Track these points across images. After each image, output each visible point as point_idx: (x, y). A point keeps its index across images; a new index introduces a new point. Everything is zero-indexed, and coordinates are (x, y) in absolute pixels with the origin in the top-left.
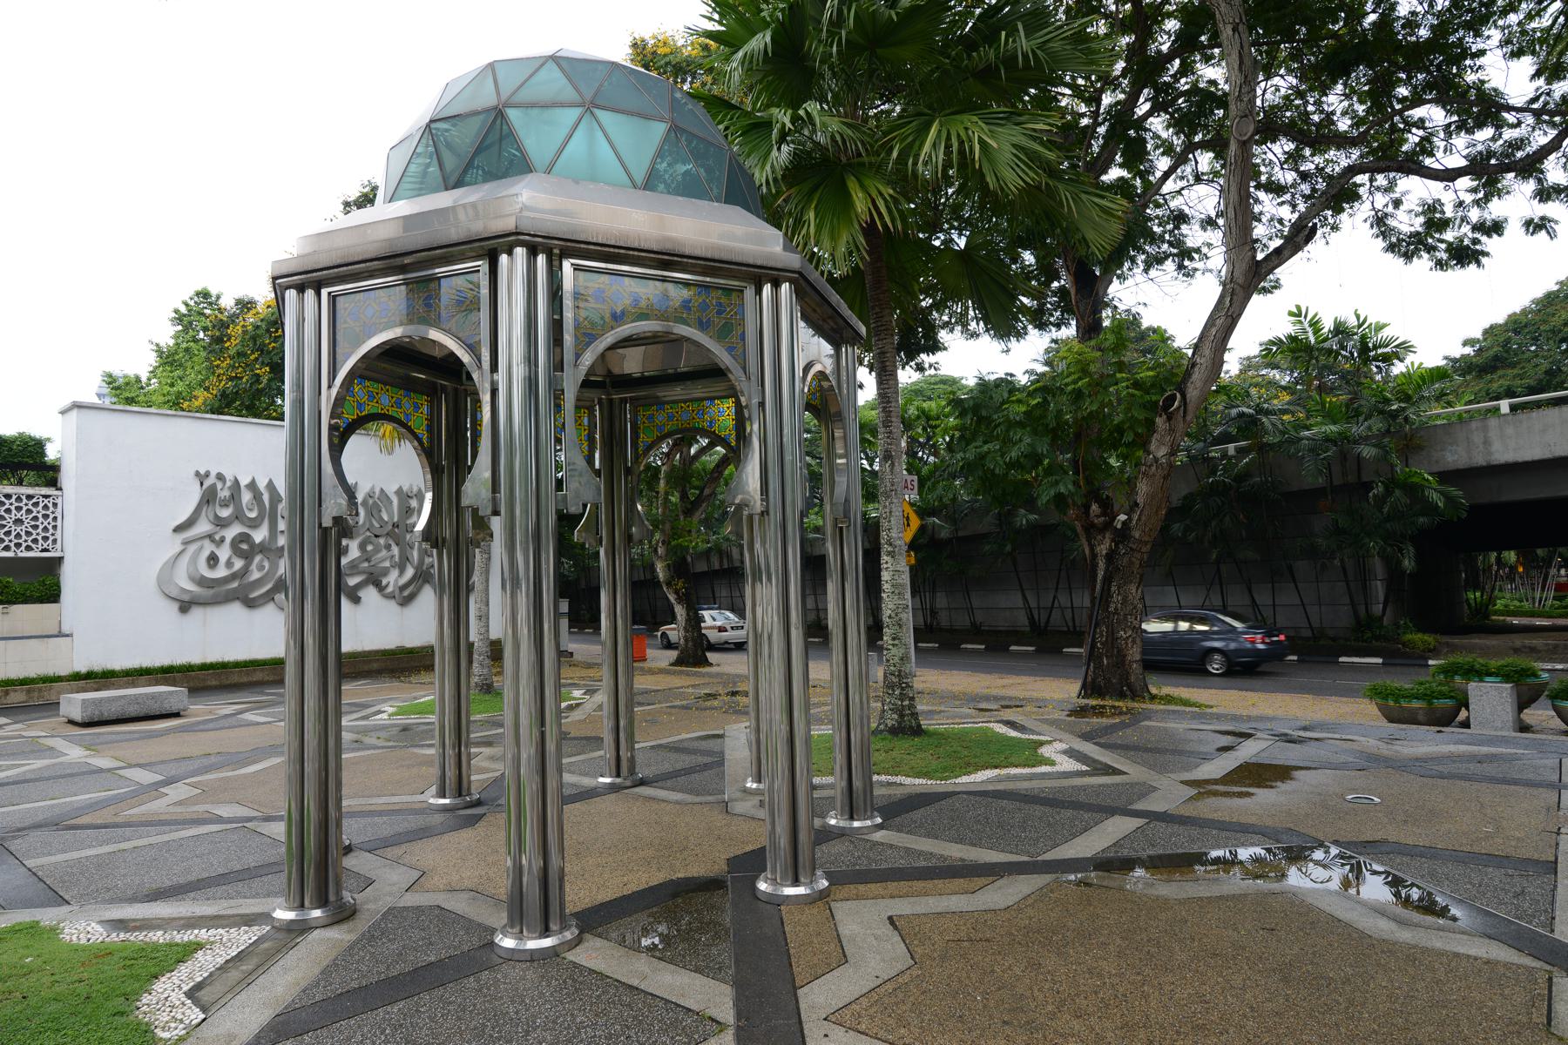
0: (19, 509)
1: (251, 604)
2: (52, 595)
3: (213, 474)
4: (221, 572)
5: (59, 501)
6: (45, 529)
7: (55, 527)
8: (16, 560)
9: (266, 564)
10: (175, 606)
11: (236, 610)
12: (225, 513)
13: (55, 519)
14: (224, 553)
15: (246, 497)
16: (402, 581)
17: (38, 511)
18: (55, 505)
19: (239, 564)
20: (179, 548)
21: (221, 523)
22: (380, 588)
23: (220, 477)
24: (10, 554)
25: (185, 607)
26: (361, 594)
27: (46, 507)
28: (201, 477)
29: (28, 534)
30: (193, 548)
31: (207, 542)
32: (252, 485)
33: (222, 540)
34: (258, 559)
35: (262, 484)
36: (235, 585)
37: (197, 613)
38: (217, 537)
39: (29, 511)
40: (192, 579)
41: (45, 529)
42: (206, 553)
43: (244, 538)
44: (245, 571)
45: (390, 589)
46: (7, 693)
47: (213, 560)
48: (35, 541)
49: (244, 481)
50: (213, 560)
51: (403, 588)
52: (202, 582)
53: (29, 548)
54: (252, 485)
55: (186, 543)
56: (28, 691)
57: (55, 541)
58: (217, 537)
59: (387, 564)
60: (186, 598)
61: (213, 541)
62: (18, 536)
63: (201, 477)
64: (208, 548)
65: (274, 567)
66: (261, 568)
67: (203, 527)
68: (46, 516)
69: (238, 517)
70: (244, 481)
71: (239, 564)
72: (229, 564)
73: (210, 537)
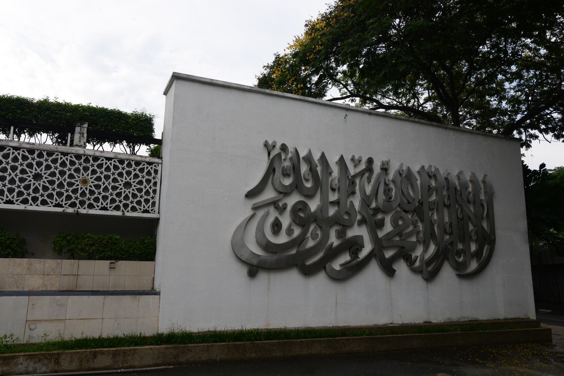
0: (86, 169)
1: (308, 272)
2: (148, 253)
3: (278, 145)
4: (282, 239)
5: (159, 168)
6: (147, 193)
7: (155, 191)
8: (123, 219)
9: (319, 232)
10: (243, 271)
11: (293, 277)
12: (287, 182)
13: (155, 184)
14: (286, 221)
15: (304, 168)
16: (428, 256)
17: (143, 177)
18: (156, 172)
19: (297, 232)
20: (249, 213)
21: (285, 192)
22: (410, 262)
23: (284, 148)
24: (119, 213)
25: (254, 269)
26: (395, 267)
27: (149, 173)
28: (268, 147)
29: (45, 188)
30: (261, 213)
31: (272, 209)
32: (308, 159)
33: (285, 207)
34: (312, 227)
35: (316, 157)
36: (294, 252)
37: (263, 277)
38: (280, 204)
39: (48, 167)
40: (259, 244)
41: (147, 193)
42: (271, 220)
43: (301, 207)
44: (302, 239)
45: (417, 264)
46: (95, 355)
47: (277, 227)
48: (50, 196)
49: (302, 154)
50: (277, 227)
51: (429, 263)
52: (268, 247)
53: (134, 209)
54: (308, 159)
55: (256, 208)
56: (115, 355)
57: (154, 204)
58: (280, 204)
59: (414, 239)
60: (255, 262)
61: (277, 208)
62: (36, 190)
63: (268, 147)
64: (273, 214)
65: (326, 236)
66: (314, 237)
67: (269, 194)
68: (148, 181)
69: (297, 186)
70: (302, 154)
71: (297, 232)
72: (290, 231)
73: (274, 203)
